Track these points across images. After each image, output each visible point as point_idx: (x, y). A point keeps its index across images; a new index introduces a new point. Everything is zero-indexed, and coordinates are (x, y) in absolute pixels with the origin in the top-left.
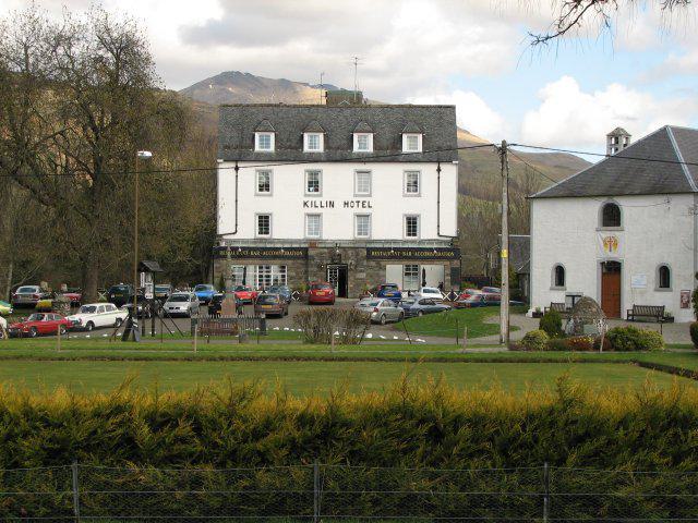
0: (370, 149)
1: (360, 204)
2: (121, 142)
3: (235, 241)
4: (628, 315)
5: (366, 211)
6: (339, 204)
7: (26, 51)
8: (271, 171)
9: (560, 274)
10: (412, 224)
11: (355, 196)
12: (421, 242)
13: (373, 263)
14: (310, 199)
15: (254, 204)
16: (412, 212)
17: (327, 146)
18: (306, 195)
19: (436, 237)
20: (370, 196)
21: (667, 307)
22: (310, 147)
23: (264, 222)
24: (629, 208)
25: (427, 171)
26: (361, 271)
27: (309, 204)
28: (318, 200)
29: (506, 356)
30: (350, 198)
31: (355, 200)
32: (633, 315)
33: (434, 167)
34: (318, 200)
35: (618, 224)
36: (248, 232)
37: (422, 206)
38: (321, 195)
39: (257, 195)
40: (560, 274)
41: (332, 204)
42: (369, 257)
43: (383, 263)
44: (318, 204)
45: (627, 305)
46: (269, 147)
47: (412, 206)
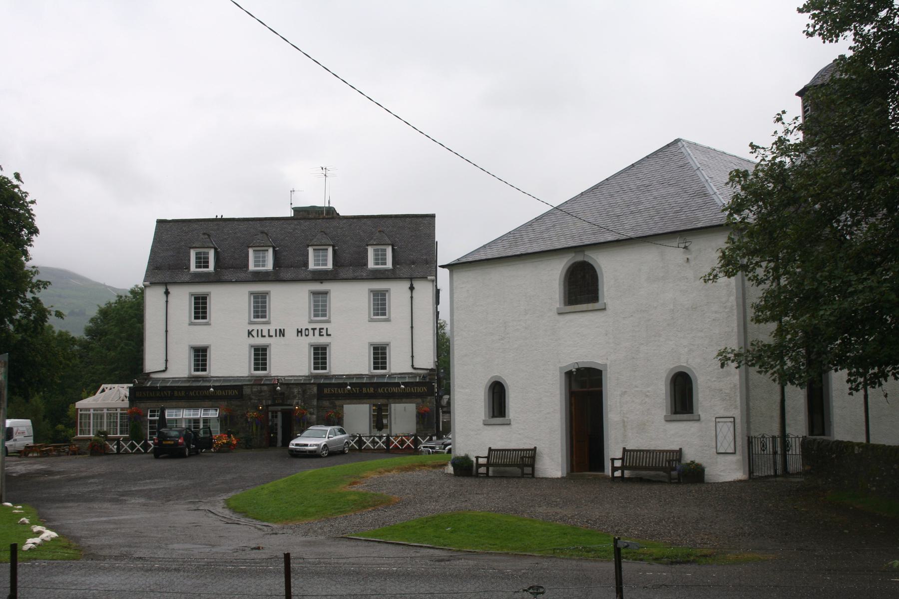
0: (269, 266)
1: (317, 332)
2: (768, 175)
3: (164, 380)
4: (614, 469)
5: (323, 340)
6: (291, 333)
8: (267, 293)
10: (380, 354)
11: (311, 322)
12: (391, 376)
13: (326, 403)
14: (255, 327)
16: (379, 339)
17: (276, 263)
18: (251, 323)
19: (411, 370)
21: (686, 451)
22: (255, 266)
23: (200, 355)
24: (172, 289)
25: (397, 292)
27: (254, 333)
28: (265, 328)
30: (304, 324)
31: (310, 327)
33: (406, 285)
34: (265, 328)
38: (268, 323)
39: (191, 324)
41: (282, 333)
42: (320, 396)
43: (338, 403)
44: (265, 333)
45: (613, 449)
47: (380, 333)
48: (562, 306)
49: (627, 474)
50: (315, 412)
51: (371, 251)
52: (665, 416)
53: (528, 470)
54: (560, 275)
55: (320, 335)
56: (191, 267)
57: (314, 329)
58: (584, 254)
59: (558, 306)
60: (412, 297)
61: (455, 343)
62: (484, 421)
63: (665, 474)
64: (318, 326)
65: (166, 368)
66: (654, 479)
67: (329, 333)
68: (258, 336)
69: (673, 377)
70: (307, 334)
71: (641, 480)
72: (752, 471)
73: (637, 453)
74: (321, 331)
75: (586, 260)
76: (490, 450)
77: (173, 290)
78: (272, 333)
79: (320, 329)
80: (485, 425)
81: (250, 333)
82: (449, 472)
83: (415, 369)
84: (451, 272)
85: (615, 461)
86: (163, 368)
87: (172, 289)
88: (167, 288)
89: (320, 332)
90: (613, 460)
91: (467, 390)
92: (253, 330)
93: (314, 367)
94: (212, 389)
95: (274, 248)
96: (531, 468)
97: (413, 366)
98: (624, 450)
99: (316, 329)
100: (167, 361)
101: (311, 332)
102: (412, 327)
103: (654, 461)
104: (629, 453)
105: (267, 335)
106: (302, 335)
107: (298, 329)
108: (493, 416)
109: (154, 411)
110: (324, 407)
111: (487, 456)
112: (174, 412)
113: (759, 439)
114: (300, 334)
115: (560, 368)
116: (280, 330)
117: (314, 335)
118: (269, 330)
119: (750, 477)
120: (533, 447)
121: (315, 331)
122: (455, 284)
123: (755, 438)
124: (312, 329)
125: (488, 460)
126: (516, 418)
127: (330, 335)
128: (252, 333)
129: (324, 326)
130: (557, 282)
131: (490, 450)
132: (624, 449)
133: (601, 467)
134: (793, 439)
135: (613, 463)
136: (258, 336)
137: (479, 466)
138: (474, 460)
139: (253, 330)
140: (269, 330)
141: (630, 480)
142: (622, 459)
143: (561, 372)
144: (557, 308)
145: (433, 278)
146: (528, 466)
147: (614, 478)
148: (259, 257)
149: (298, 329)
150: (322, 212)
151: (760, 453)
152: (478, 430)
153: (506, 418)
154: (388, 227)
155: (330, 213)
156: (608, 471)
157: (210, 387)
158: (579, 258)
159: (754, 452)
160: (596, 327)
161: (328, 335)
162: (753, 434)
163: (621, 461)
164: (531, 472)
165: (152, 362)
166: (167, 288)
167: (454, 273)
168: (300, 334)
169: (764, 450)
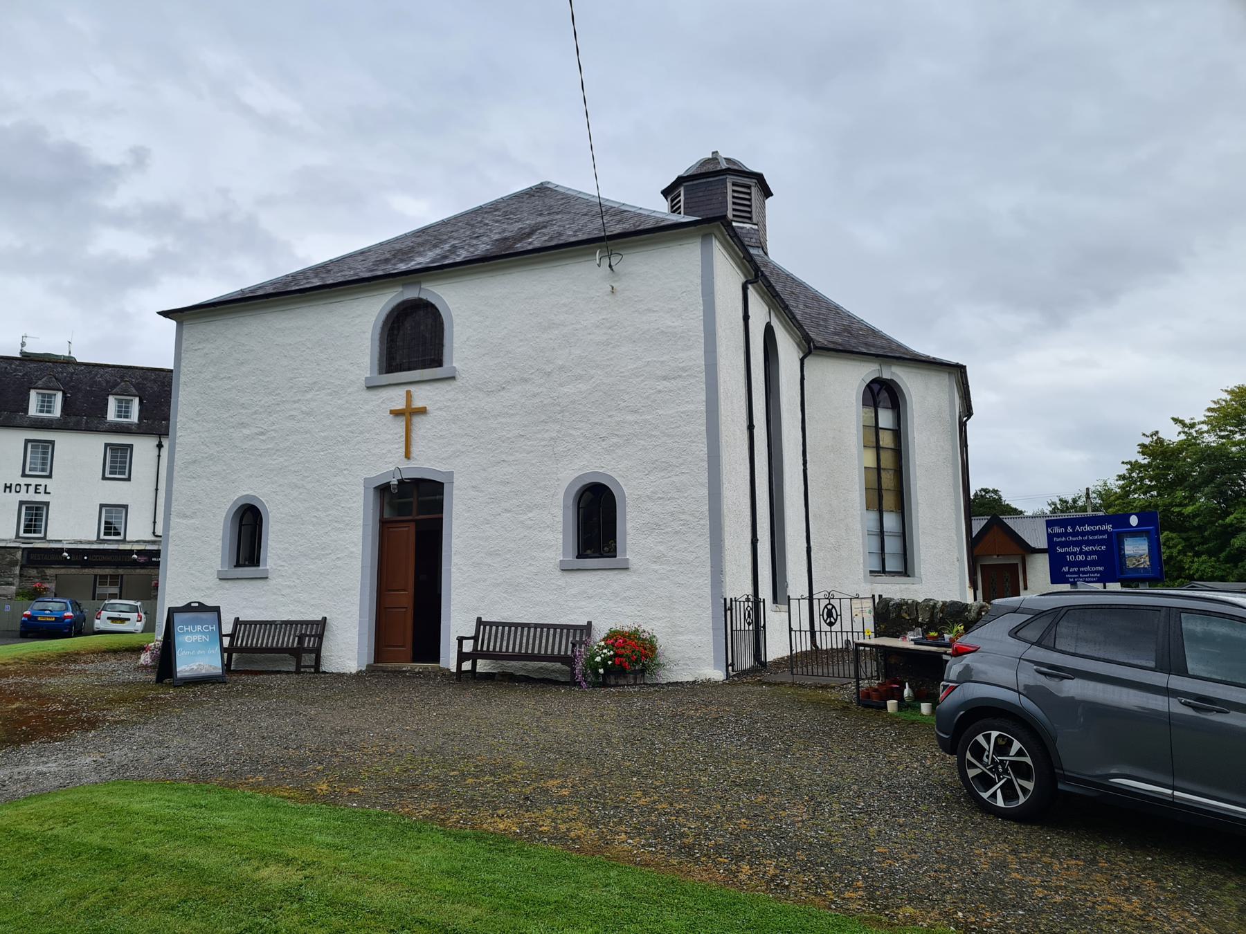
1: (32, 489)
4: (462, 656)
5: (41, 498)
13: (33, 572)
20: (50, 476)
30: (15, 478)
32: (474, 656)
47: (116, 492)
48: (376, 374)
49: (483, 666)
51: (112, 403)
53: (308, 659)
55: (36, 492)
57: (28, 485)
58: (420, 288)
60: (159, 456)
62: (219, 571)
63: (565, 667)
67: (48, 491)
69: (584, 486)
70: (18, 490)
71: (509, 679)
73: (510, 628)
74: (38, 487)
75: (423, 296)
79: (36, 485)
83: (157, 536)
84: (180, 325)
85: (465, 642)
89: (36, 489)
91: (192, 521)
93: (24, 530)
97: (154, 533)
99: (31, 485)
101: (24, 488)
104: (488, 628)
106: (10, 491)
107: (6, 484)
108: (238, 565)
110: (30, 577)
111: (230, 633)
113: (742, 604)
114: (8, 490)
117: (27, 492)
121: (30, 487)
122: (184, 346)
123: (736, 601)
124: (25, 485)
126: (279, 568)
127: (49, 493)
130: (369, 335)
132: (479, 620)
134: (846, 603)
141: (488, 677)
142: (475, 638)
144: (366, 378)
146: (309, 651)
149: (6, 484)
151: (747, 628)
152: (207, 588)
153: (261, 568)
154: (137, 379)
156: (449, 660)
158: (411, 294)
159: (734, 629)
160: (437, 409)
161: (46, 493)
163: (472, 641)
167: (184, 326)
168: (8, 490)
169: (831, 624)
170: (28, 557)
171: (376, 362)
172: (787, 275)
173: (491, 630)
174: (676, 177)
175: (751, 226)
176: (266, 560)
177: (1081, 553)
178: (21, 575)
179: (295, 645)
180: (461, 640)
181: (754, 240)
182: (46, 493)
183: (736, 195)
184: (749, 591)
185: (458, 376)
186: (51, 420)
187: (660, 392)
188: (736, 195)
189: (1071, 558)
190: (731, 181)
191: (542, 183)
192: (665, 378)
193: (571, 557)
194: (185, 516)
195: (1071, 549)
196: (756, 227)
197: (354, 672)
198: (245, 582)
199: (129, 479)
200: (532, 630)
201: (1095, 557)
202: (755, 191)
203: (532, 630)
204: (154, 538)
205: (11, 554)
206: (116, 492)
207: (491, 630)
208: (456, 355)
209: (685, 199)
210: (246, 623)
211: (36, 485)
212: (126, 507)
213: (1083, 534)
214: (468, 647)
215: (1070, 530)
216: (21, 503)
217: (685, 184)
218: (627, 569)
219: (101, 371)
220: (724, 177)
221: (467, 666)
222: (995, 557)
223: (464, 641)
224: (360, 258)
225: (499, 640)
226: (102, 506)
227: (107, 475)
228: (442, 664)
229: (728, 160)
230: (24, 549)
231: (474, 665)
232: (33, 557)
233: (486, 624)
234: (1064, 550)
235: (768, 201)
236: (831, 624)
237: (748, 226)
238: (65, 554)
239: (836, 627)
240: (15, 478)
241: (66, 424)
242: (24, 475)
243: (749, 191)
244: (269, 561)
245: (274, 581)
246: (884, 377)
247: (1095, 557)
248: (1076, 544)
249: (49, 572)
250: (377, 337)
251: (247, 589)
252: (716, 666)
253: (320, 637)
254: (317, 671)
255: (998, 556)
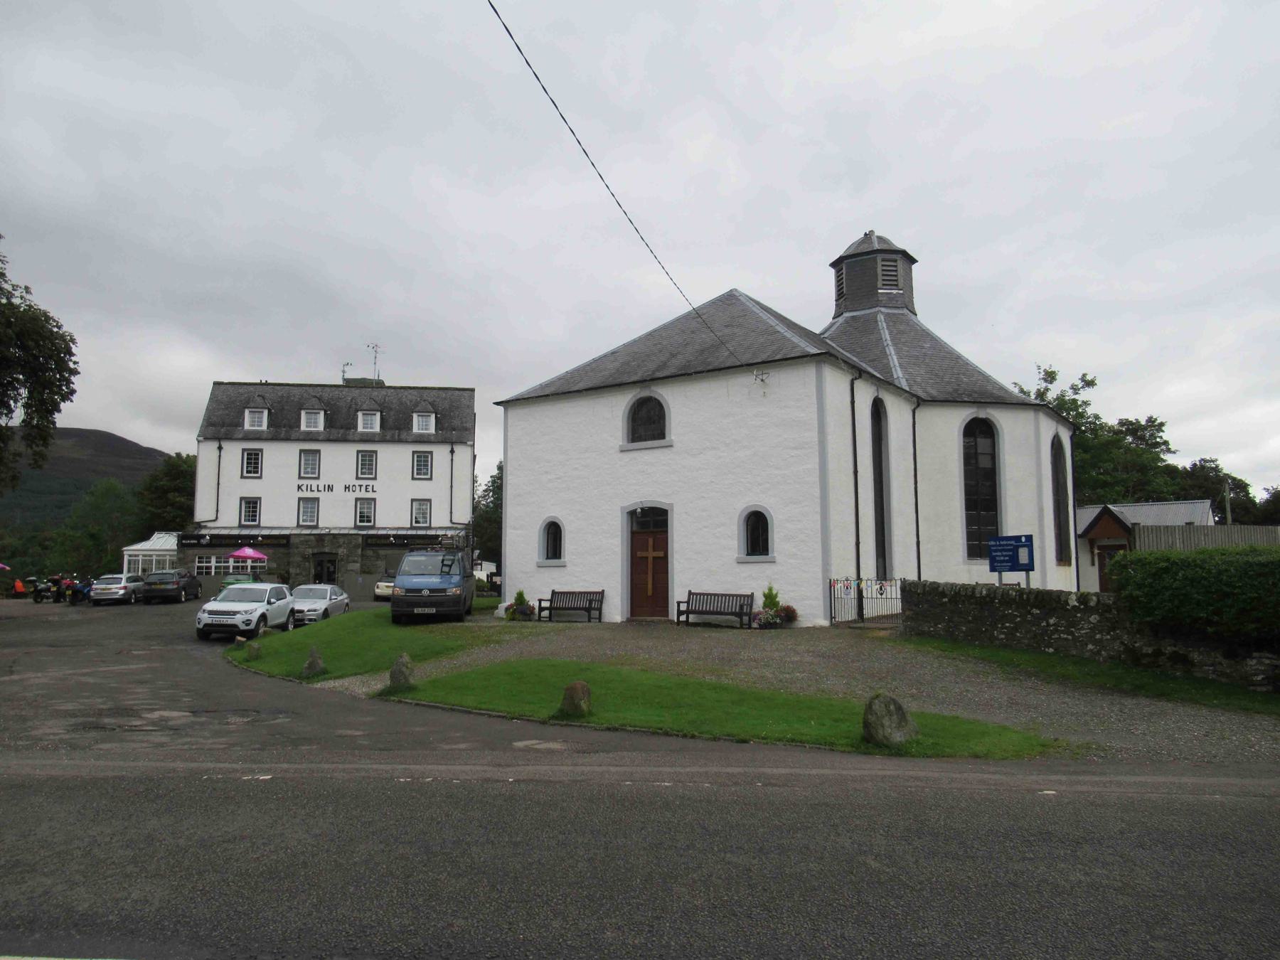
1: (363, 488)
4: (680, 613)
6: (339, 488)
7: (1149, 793)
9: (553, 537)
13: (370, 553)
15: (237, 487)
20: (375, 478)
25: (440, 454)
26: (354, 562)
28: (314, 483)
29: (887, 390)
30: (352, 481)
32: (688, 612)
33: (447, 448)
35: (661, 435)
36: (229, 520)
37: (434, 489)
40: (553, 537)
41: (330, 488)
44: (314, 488)
45: (678, 593)
46: (261, 426)
47: (422, 489)
48: (625, 443)
49: (692, 618)
50: (360, 560)
52: (737, 558)
53: (595, 614)
54: (624, 413)
56: (245, 425)
59: (621, 443)
60: (452, 460)
61: (508, 482)
63: (736, 618)
64: (364, 483)
65: (217, 518)
66: (724, 625)
68: (307, 490)
72: (833, 615)
76: (554, 593)
77: (225, 445)
78: (321, 488)
80: (539, 567)
81: (299, 487)
82: (501, 616)
86: (214, 518)
87: (224, 444)
88: (220, 444)
89: (366, 489)
90: (679, 603)
92: (302, 485)
94: (260, 538)
95: (325, 412)
96: (598, 612)
97: (451, 520)
98: (690, 593)
100: (217, 511)
101: (358, 488)
102: (452, 486)
103: (723, 605)
105: (316, 490)
108: (548, 558)
109: (220, 558)
112: (431, 612)
114: (347, 490)
115: (622, 508)
116: (329, 486)
117: (360, 491)
118: (318, 486)
119: (832, 624)
120: (601, 590)
122: (510, 423)
125: (688, 606)
127: (375, 491)
128: (302, 487)
129: (371, 483)
130: (621, 418)
131: (554, 593)
132: (690, 592)
133: (664, 610)
135: (679, 606)
136: (307, 490)
137: (541, 609)
138: (537, 604)
139: (302, 485)
140: (318, 486)
141: (696, 625)
142: (688, 602)
143: (622, 513)
145: (472, 443)
146: (594, 609)
147: (679, 622)
148: (311, 419)
150: (373, 383)
155: (380, 385)
156: (673, 615)
157: (258, 536)
158: (645, 393)
159: (836, 597)
161: (373, 491)
162: (834, 577)
163: (686, 604)
164: (598, 617)
165: (203, 511)
166: (220, 444)
168: (347, 490)
169: (881, 594)
170: (366, 541)
171: (625, 436)
172: (924, 330)
173: (696, 597)
174: (838, 256)
175: (897, 291)
176: (564, 556)
177: (1002, 556)
178: (362, 556)
179: (587, 606)
180: (679, 603)
181: (899, 303)
182: (373, 491)
183: (884, 268)
184: (852, 573)
185: (674, 445)
186: (374, 434)
187: (792, 456)
188: (884, 268)
189: (997, 558)
190: (881, 258)
191: (731, 290)
192: (796, 448)
193: (743, 556)
194: (515, 528)
195: (999, 554)
196: (901, 292)
197: (619, 621)
198: (552, 568)
199: (431, 479)
200: (720, 597)
201: (1007, 558)
202: (901, 264)
203: (720, 597)
204: (450, 525)
205: (355, 539)
206: (422, 489)
207: (696, 597)
208: (673, 431)
209: (846, 273)
210: (559, 593)
211: (366, 486)
212: (430, 501)
213: (1003, 545)
214: (683, 607)
215: (998, 543)
216: (357, 500)
217: (845, 261)
218: (774, 562)
219: (406, 393)
220: (875, 255)
221: (683, 618)
222: (1106, 540)
223: (681, 604)
224: (612, 358)
225: (708, 604)
226: (413, 500)
227: (415, 476)
228: (670, 617)
229: (880, 238)
230: (363, 535)
231: (688, 617)
232: (369, 541)
233: (694, 594)
234: (996, 554)
235: (914, 267)
236: (881, 594)
237: (894, 292)
238: (392, 539)
239: (884, 596)
240: (352, 481)
241: (382, 439)
242: (357, 478)
243: (895, 264)
244: (566, 556)
245: (570, 568)
246: (980, 417)
247: (1007, 558)
248: (1001, 551)
249: (382, 552)
250: (626, 415)
251: (556, 573)
252: (825, 619)
253: (601, 602)
254: (600, 621)
255: (1108, 538)
